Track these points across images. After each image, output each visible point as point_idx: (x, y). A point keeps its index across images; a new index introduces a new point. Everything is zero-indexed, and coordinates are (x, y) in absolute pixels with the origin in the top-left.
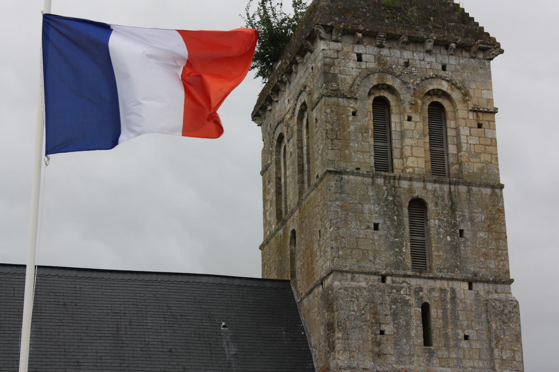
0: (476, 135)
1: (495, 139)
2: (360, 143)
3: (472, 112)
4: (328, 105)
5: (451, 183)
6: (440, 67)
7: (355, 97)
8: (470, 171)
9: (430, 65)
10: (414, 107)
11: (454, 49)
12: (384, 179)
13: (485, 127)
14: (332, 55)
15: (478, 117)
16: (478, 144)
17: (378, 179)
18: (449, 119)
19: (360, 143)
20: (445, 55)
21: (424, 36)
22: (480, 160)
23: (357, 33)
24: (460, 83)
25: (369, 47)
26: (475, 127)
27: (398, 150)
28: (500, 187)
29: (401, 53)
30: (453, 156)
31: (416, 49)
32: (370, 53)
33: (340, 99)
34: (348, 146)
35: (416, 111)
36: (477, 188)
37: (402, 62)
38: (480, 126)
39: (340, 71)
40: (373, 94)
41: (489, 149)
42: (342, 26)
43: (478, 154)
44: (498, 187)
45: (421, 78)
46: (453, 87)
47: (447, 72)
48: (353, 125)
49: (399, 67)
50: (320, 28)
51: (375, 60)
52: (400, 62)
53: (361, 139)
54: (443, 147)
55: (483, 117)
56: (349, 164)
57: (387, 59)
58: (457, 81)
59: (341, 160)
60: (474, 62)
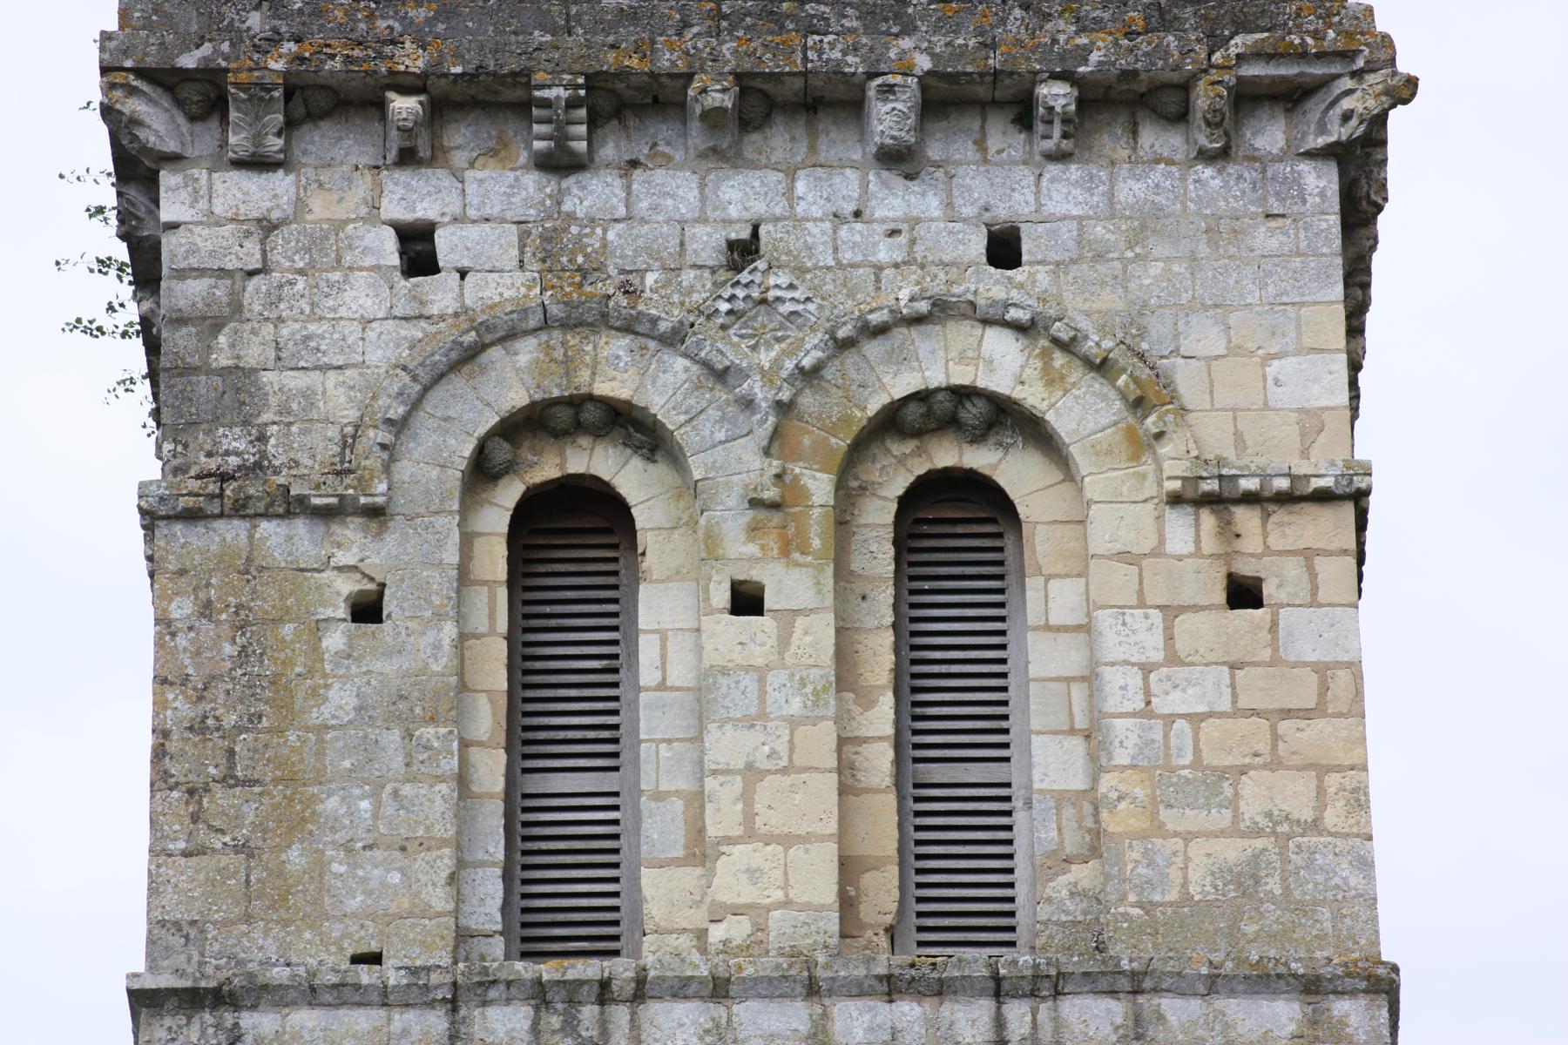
0: (1210, 657)
1: (1355, 669)
2: (388, 789)
3: (1189, 509)
4: (182, 572)
5: (1006, 986)
6: (977, 245)
7: (363, 500)
8: (1157, 898)
9: (902, 239)
10: (776, 518)
11: (1066, 121)
12: (537, 1009)
13: (1283, 596)
14: (227, 252)
15: (1229, 534)
16: (1221, 715)
17: (493, 1013)
18: (1039, 571)
19: (388, 789)
20: (1014, 163)
21: (850, 59)
22: (1236, 816)
23: (391, 95)
24: (1102, 329)
25: (479, 174)
26: (1203, 602)
27: (678, 805)
28: (1364, 985)
29: (702, 186)
30: (1058, 808)
31: (813, 148)
32: (488, 211)
33: (266, 527)
34: (304, 819)
35: (788, 548)
36: (1195, 1004)
37: (708, 243)
38: (1243, 594)
39: (278, 349)
40: (510, 468)
41: (1301, 737)
42: (278, 65)
43: (1222, 778)
44: (1349, 983)
45: (832, 333)
46: (1059, 359)
47: (1018, 274)
48: (345, 678)
49: (688, 276)
50: (132, 91)
51: (522, 253)
52: (691, 247)
53: (398, 763)
54: (1007, 760)
55: (1265, 536)
56: (307, 935)
57: (604, 238)
58: (1084, 324)
59: (248, 918)
60: (1217, 183)
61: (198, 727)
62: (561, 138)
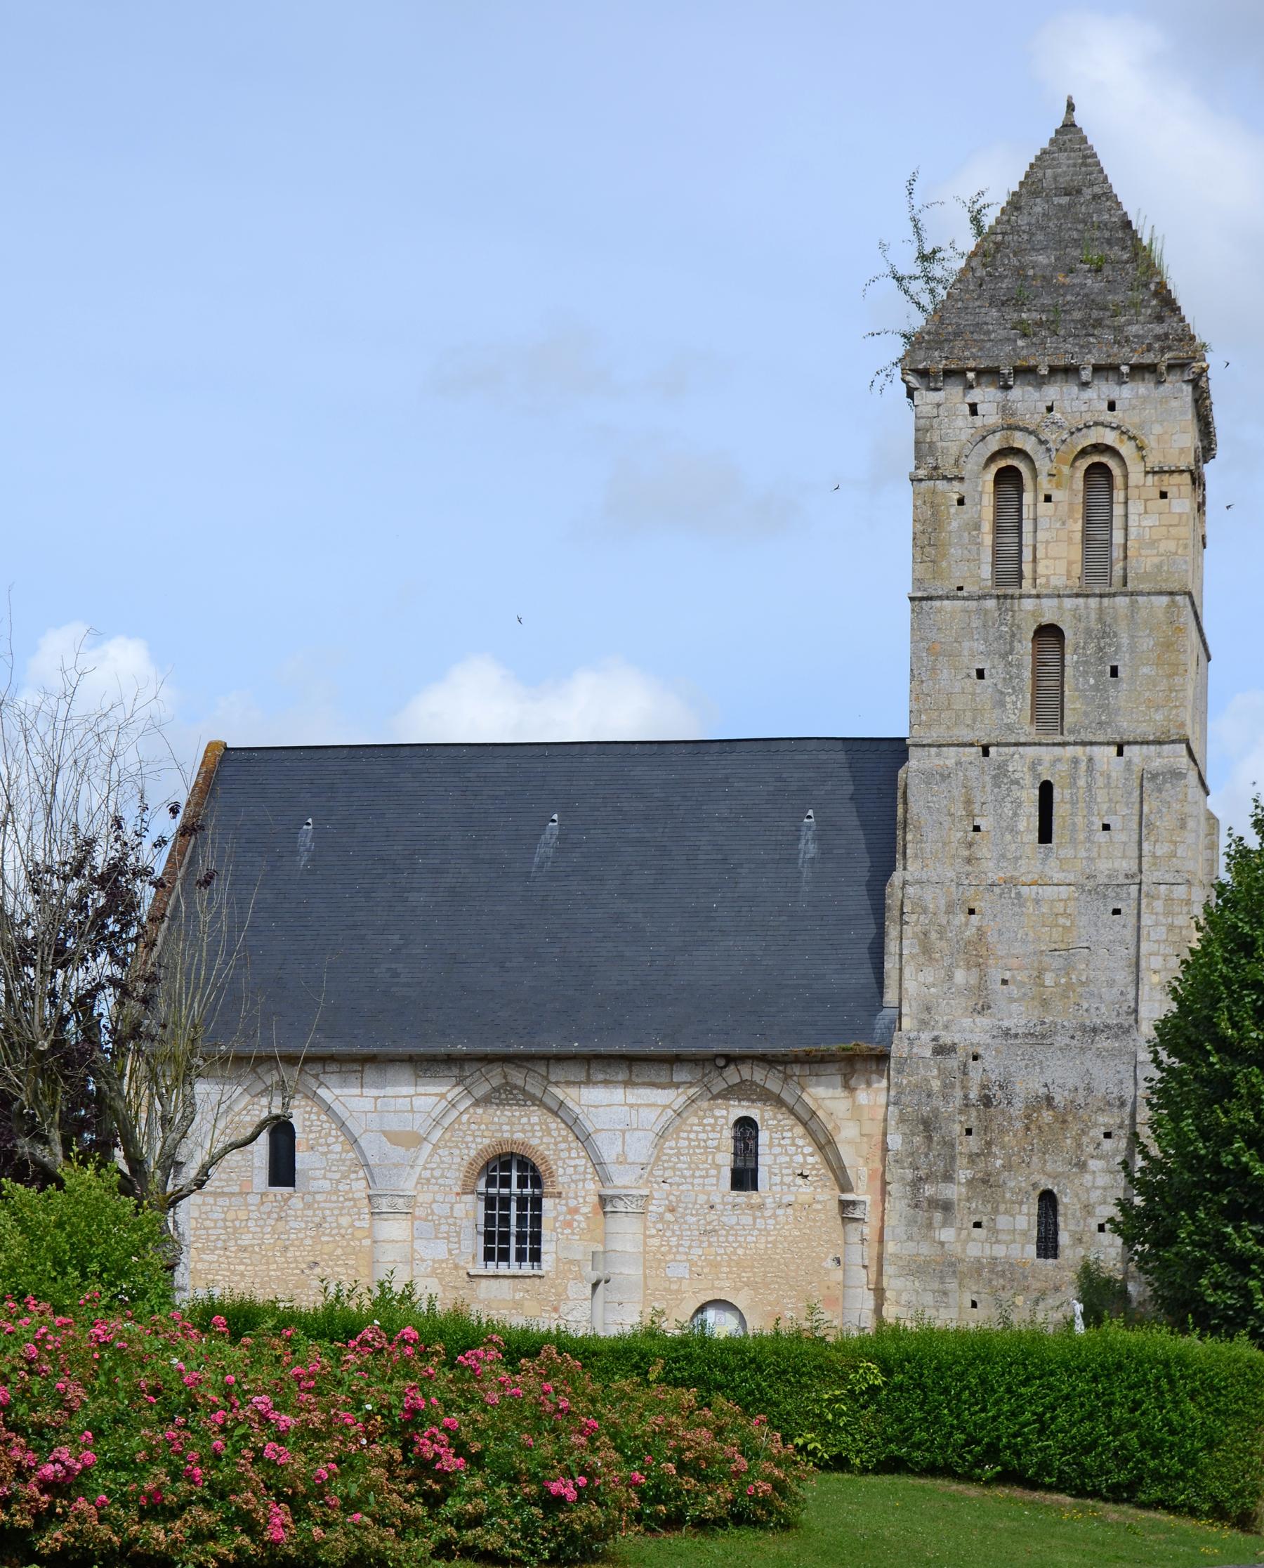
6: (1106, 405)
38: (1163, 495)
61: (923, 532)
62: (1006, 382)
